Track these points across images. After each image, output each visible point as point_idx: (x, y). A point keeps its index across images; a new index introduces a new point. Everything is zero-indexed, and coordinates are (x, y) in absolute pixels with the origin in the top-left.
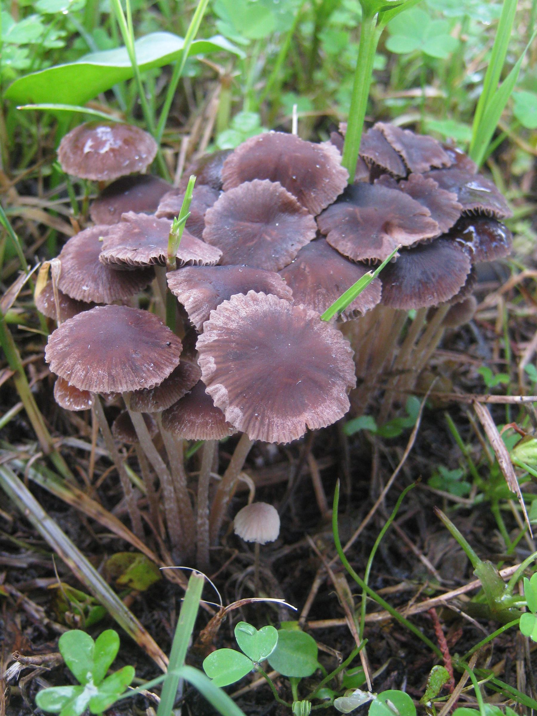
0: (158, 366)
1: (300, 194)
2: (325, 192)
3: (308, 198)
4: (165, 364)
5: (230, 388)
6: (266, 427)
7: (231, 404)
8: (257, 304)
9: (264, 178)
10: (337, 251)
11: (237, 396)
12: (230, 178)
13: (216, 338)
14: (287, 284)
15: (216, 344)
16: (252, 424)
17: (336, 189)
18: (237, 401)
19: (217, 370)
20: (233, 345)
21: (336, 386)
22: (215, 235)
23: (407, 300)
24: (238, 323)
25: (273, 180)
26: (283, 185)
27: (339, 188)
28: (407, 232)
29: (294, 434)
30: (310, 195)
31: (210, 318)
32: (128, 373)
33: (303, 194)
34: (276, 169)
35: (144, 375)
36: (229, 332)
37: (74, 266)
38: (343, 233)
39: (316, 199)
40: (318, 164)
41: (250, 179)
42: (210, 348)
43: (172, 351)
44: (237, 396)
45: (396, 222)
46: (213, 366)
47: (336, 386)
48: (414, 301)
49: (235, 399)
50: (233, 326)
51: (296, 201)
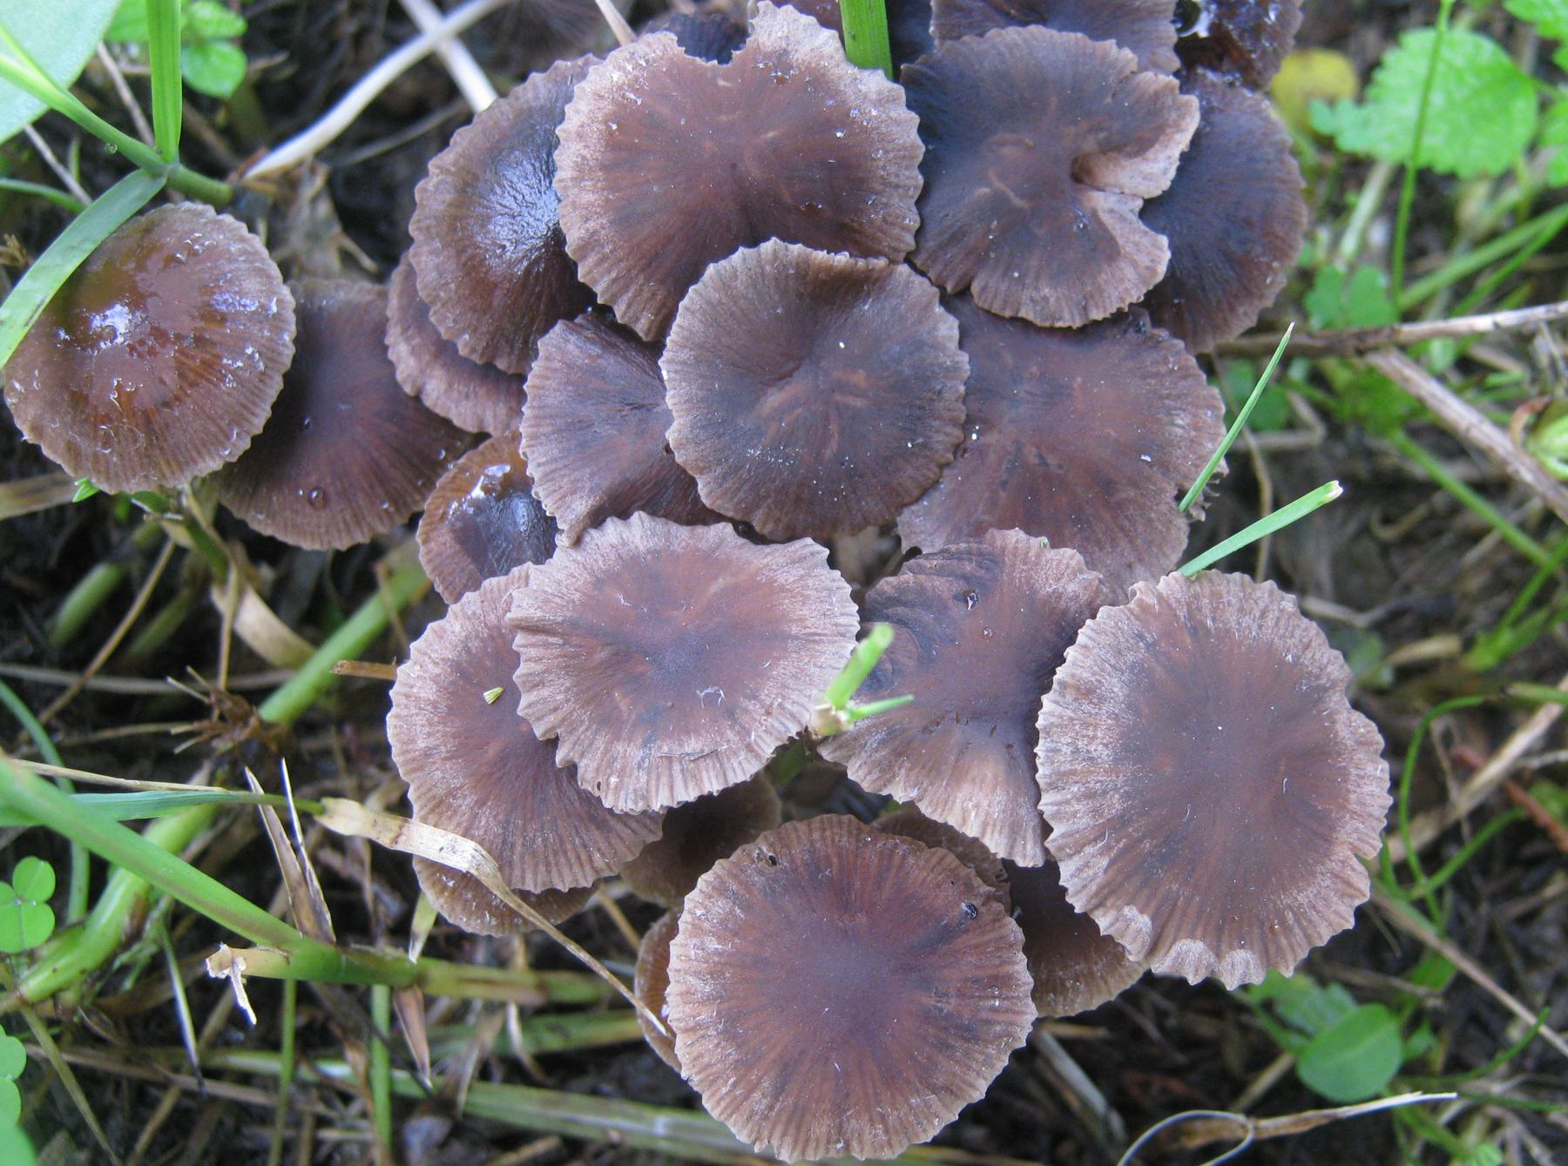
0: (1003, 982)
1: (842, 234)
2: (897, 186)
3: (869, 231)
4: (1003, 963)
5: (1199, 931)
6: (1297, 930)
7: (1219, 956)
8: (1102, 699)
9: (733, 251)
10: (1026, 324)
11: (1220, 930)
12: (626, 288)
13: (1105, 862)
14: (1054, 546)
15: (1111, 872)
16: (1272, 949)
17: (905, 155)
18: (1225, 938)
19: (1153, 919)
20: (1147, 845)
21: (1124, 544)
22: (738, 489)
23: (1225, 320)
24: (1116, 789)
25: (754, 242)
26: (790, 238)
27: (913, 147)
28: (1131, 155)
29: (1351, 896)
30: (871, 222)
31: (1052, 824)
32: (967, 1054)
33: (853, 230)
34: (745, 209)
35: (998, 1028)
36: (1119, 824)
37: (508, 822)
38: (1007, 271)
39: (890, 219)
40: (837, 129)
41: (695, 276)
42: (1106, 894)
43: (988, 918)
44: (1220, 930)
45: (1089, 145)
46: (1143, 922)
47: (1124, 544)
48: (1241, 310)
49: (1219, 940)
50: (1115, 805)
51: (852, 261)
